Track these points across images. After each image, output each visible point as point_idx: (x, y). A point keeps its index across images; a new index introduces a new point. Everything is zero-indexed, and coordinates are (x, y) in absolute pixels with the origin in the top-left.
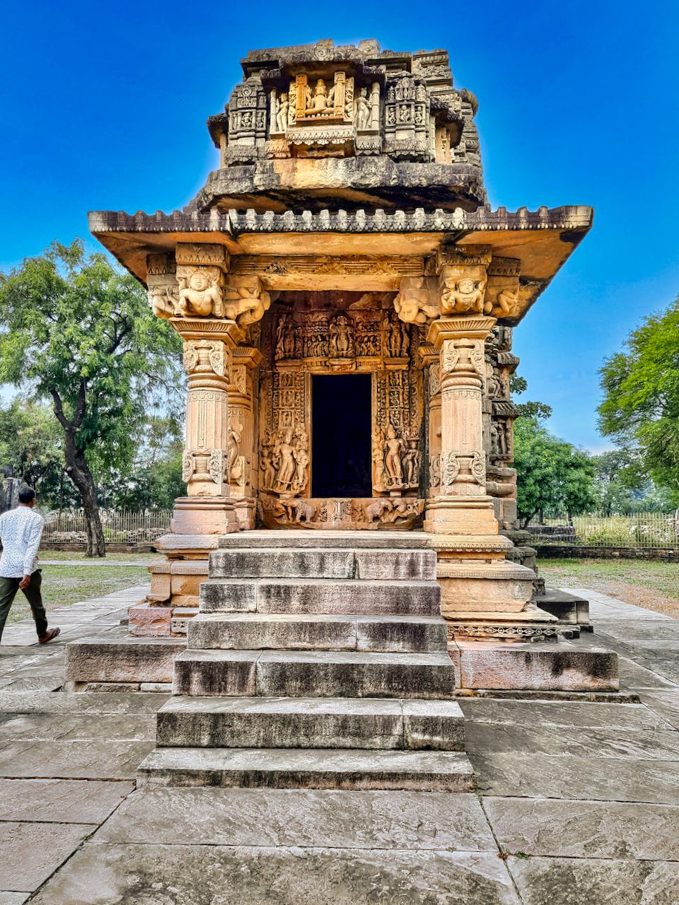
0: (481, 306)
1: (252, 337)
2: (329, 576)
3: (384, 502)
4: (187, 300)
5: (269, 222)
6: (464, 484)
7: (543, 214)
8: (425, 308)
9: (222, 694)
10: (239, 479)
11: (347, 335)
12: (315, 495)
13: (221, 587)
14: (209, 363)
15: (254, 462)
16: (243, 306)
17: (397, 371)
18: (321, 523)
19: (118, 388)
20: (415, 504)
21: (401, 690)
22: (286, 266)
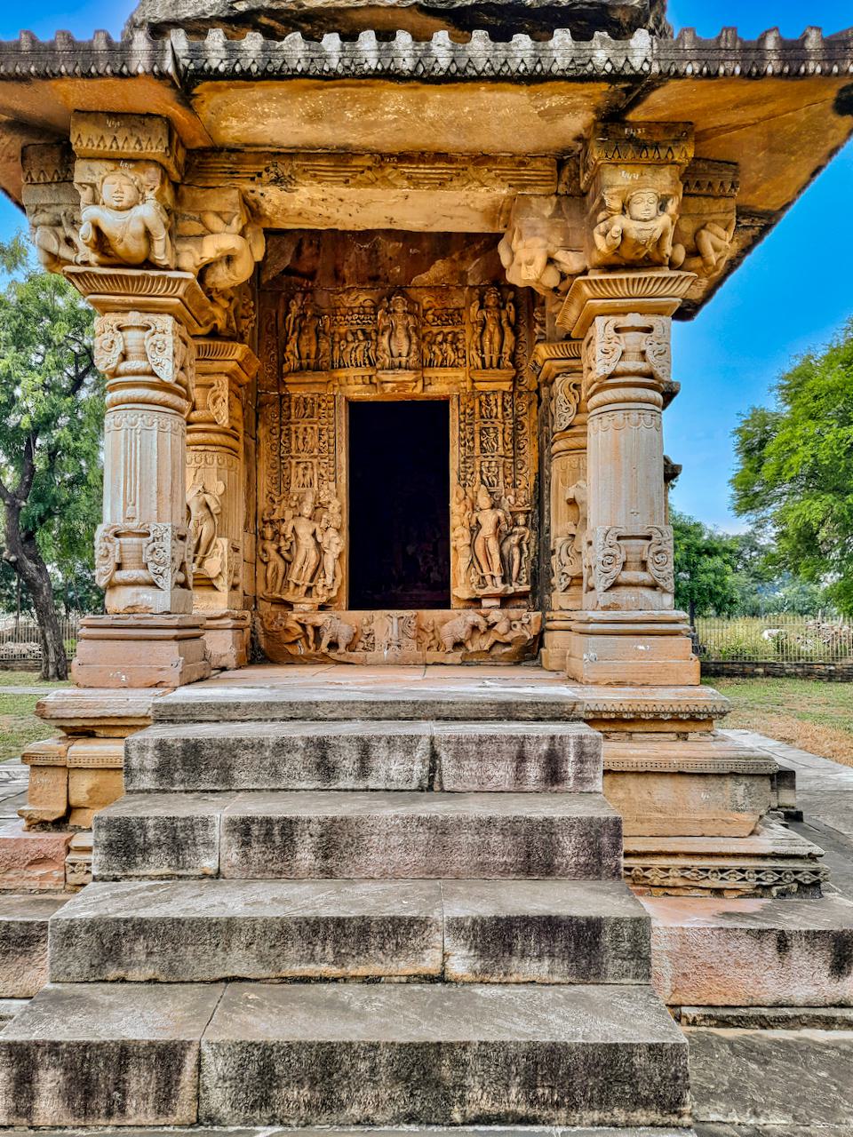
0: (668, 250)
1: (238, 324)
2: (380, 785)
3: (473, 617)
4: (97, 229)
5: (252, 55)
6: (633, 590)
7: (813, 43)
8: (560, 255)
9: (115, 1121)
10: (217, 578)
11: (407, 329)
12: (353, 606)
13: (141, 823)
14: (144, 356)
15: (247, 550)
16: (210, 249)
17: (494, 392)
18: (364, 653)
19: (78, 445)
20: (525, 621)
21: (558, 1105)
22: (293, 171)
